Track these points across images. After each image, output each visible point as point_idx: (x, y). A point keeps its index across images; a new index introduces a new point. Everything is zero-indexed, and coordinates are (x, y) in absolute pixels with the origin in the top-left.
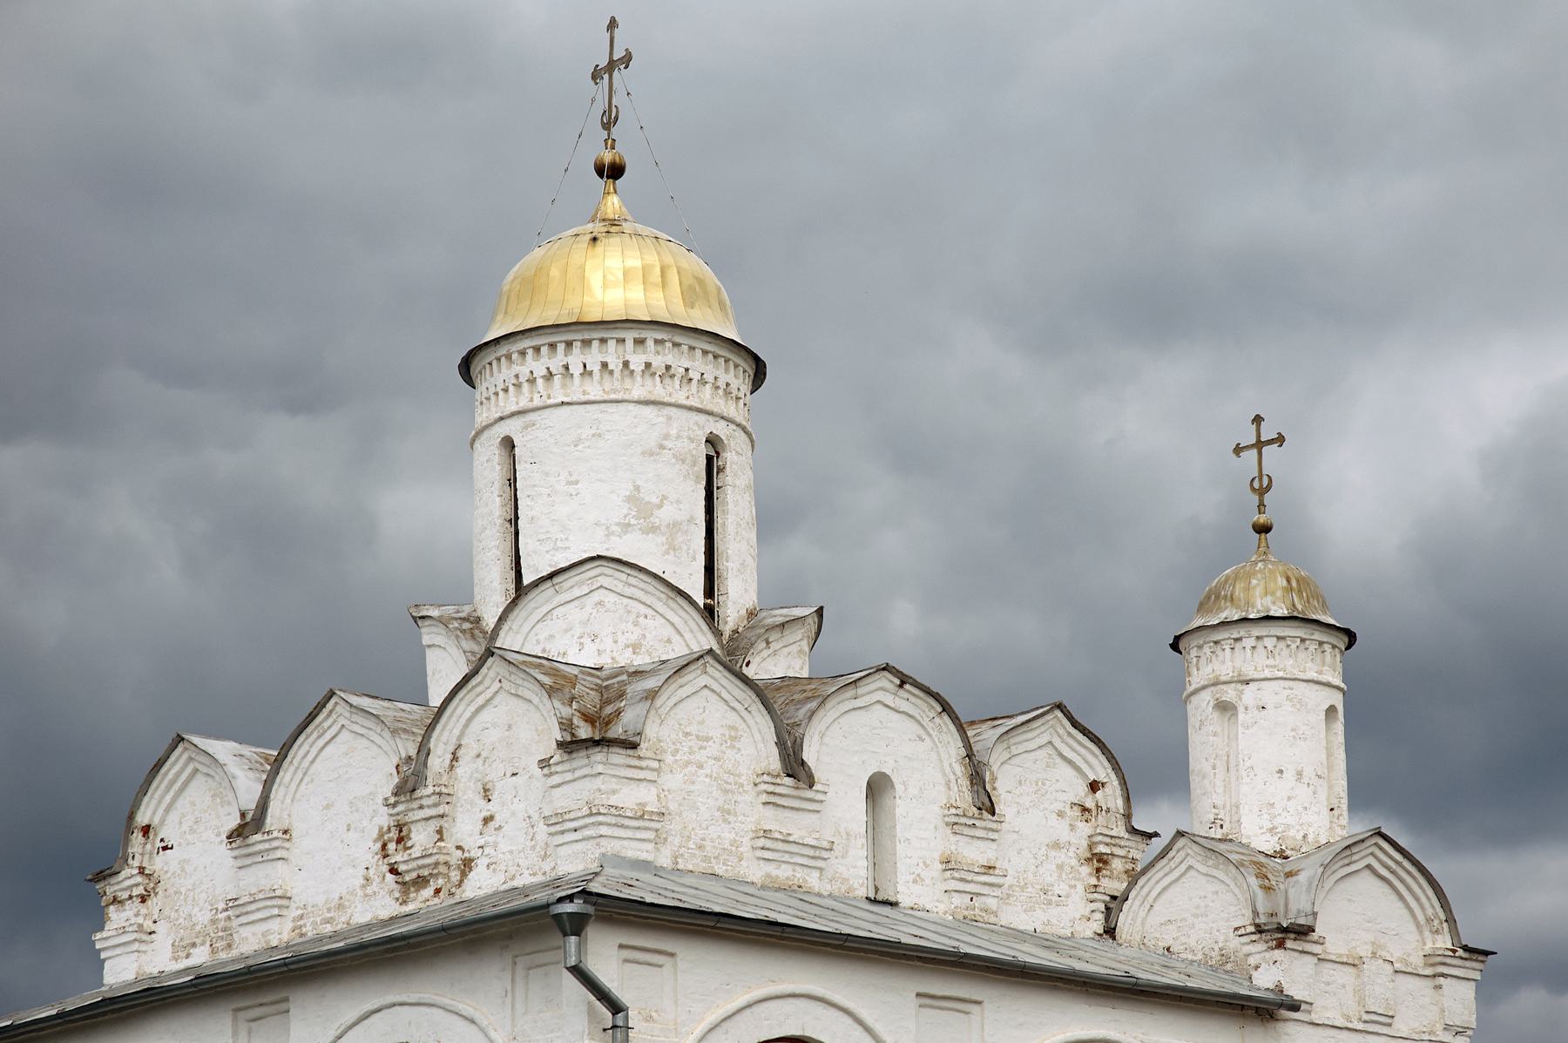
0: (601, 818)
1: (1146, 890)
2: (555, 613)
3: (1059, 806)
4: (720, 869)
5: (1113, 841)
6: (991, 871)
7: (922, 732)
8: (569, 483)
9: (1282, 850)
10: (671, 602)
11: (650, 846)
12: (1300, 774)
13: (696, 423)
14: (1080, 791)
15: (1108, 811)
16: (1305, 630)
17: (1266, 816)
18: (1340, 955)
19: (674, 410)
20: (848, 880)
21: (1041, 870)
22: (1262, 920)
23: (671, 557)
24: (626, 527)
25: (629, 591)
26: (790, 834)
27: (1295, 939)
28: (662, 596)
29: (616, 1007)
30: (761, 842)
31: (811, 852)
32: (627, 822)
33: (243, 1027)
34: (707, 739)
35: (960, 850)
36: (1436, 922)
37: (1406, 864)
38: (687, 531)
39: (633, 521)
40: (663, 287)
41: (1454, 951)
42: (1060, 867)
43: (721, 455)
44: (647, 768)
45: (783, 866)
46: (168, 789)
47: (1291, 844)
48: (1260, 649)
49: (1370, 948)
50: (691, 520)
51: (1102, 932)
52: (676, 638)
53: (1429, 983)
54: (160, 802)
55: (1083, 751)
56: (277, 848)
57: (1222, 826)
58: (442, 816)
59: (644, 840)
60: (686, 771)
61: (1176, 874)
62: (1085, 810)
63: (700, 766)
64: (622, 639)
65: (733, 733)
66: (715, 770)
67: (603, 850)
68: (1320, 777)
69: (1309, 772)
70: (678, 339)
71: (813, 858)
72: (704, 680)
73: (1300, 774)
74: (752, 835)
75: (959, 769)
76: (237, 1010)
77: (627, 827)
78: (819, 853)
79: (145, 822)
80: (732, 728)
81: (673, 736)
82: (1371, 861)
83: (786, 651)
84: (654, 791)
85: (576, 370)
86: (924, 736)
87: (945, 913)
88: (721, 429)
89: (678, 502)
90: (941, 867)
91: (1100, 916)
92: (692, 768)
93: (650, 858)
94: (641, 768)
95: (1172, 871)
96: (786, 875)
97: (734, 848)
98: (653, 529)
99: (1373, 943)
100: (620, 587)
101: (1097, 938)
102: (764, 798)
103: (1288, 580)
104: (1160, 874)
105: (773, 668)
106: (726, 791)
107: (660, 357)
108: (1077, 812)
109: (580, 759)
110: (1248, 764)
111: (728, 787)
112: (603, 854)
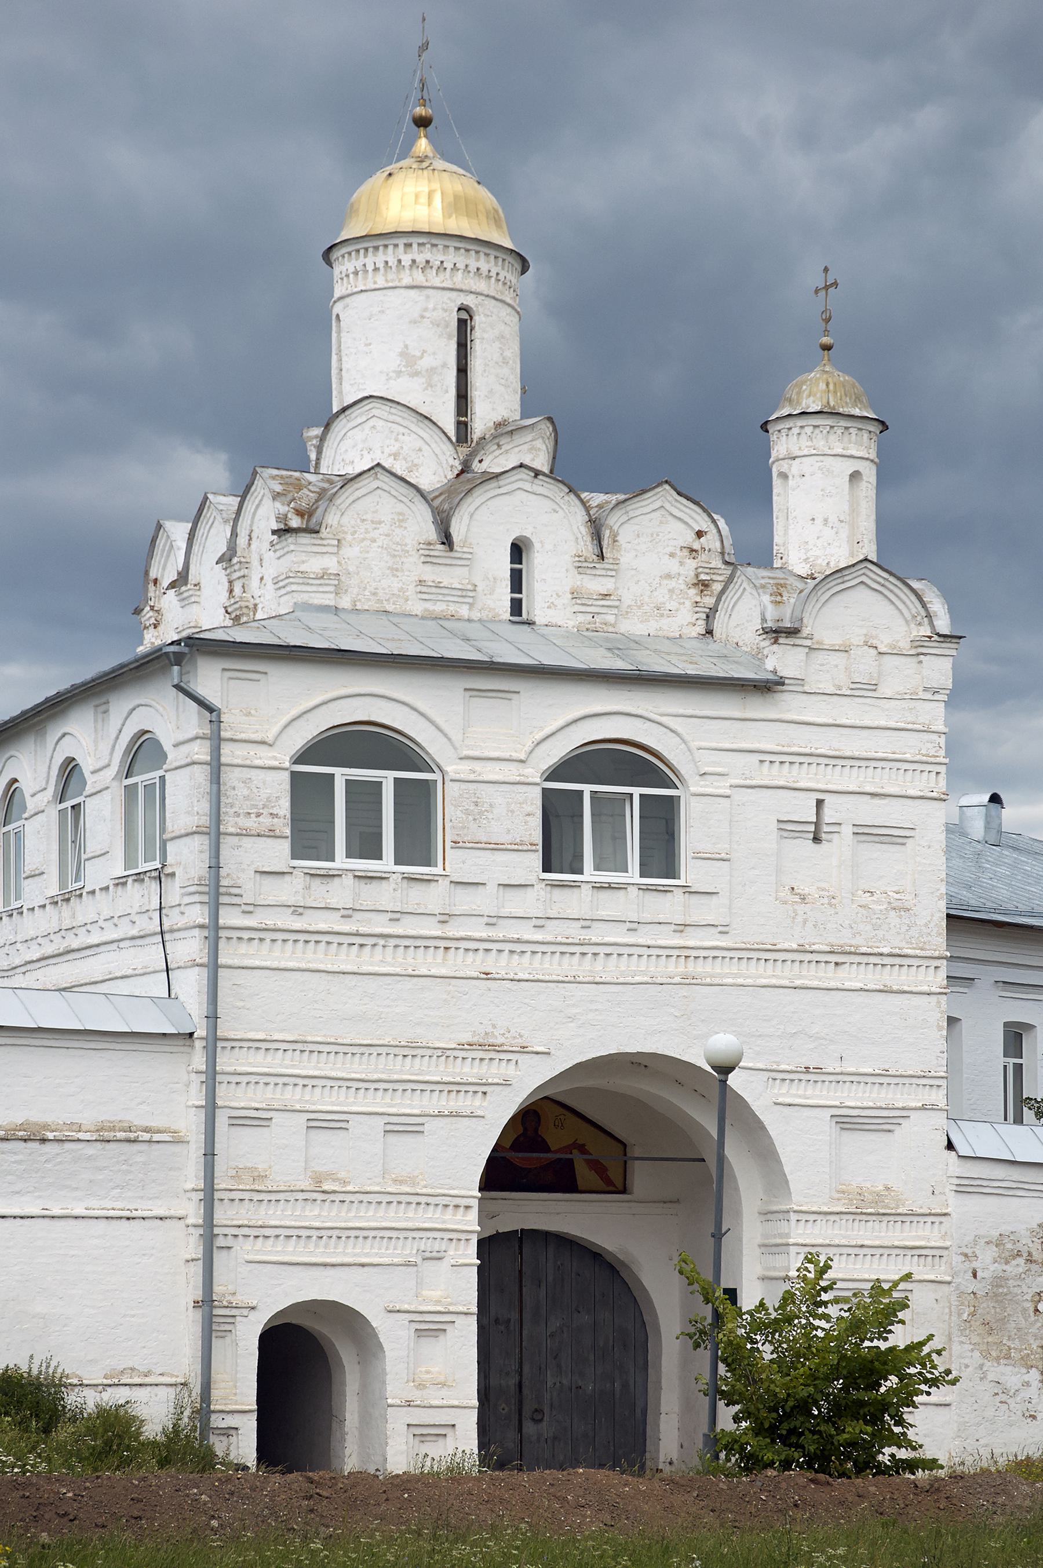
0: (291, 580)
1: (726, 604)
2: (348, 434)
3: (670, 549)
4: (390, 608)
5: (712, 571)
6: (608, 597)
7: (556, 507)
8: (367, 345)
9: (812, 574)
10: (420, 424)
11: (332, 596)
12: (826, 520)
13: (449, 299)
14: (689, 538)
15: (710, 550)
16: (832, 420)
17: (803, 551)
18: (834, 645)
19: (431, 291)
20: (494, 609)
21: (655, 594)
22: (770, 624)
23: (429, 392)
24: (399, 373)
25: (392, 418)
26: (441, 582)
27: (787, 637)
28: (414, 420)
29: (210, 709)
30: (419, 588)
31: (460, 593)
32: (311, 581)
33: (100, 716)
34: (380, 522)
35: (584, 584)
36: (919, 618)
37: (892, 579)
38: (441, 373)
39: (403, 369)
40: (429, 205)
41: (930, 637)
42: (671, 591)
43: (474, 318)
44: (328, 545)
45: (438, 603)
46: (162, 555)
47: (818, 569)
48: (803, 436)
49: (863, 639)
50: (444, 365)
51: (704, 633)
52: (425, 447)
53: (915, 659)
54: (159, 563)
55: (687, 510)
56: (192, 596)
57: (782, 558)
58: (244, 576)
59: (326, 592)
60: (362, 545)
61: (739, 593)
62: (692, 550)
63: (374, 541)
64: (387, 451)
65: (401, 517)
66: (385, 542)
67: (295, 600)
68: (842, 521)
69: (833, 519)
70: (434, 241)
71: (462, 596)
72: (376, 484)
73: (826, 520)
74: (415, 584)
75: (584, 530)
76: (97, 706)
77: (312, 585)
78: (468, 593)
79: (154, 577)
80: (400, 514)
81: (353, 522)
82: (864, 579)
83: (517, 450)
84: (335, 559)
85: (370, 267)
86: (558, 509)
87: (573, 627)
88: (470, 301)
89: (434, 354)
90: (570, 596)
91: (702, 623)
92: (367, 543)
93: (332, 603)
94: (324, 545)
95: (737, 591)
96: (441, 609)
97: (401, 594)
98: (417, 374)
99: (866, 635)
100: (385, 415)
101: (701, 637)
102: (423, 559)
103: (827, 385)
104: (732, 593)
105: (505, 462)
106: (395, 556)
107: (421, 255)
108: (686, 552)
109: (290, 539)
110: (794, 514)
111: (396, 553)
112: (295, 603)
